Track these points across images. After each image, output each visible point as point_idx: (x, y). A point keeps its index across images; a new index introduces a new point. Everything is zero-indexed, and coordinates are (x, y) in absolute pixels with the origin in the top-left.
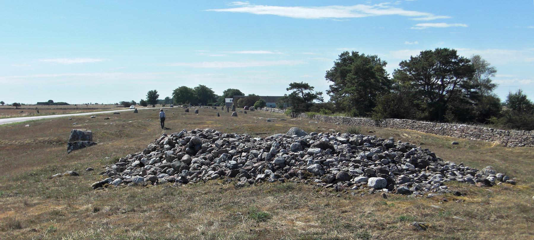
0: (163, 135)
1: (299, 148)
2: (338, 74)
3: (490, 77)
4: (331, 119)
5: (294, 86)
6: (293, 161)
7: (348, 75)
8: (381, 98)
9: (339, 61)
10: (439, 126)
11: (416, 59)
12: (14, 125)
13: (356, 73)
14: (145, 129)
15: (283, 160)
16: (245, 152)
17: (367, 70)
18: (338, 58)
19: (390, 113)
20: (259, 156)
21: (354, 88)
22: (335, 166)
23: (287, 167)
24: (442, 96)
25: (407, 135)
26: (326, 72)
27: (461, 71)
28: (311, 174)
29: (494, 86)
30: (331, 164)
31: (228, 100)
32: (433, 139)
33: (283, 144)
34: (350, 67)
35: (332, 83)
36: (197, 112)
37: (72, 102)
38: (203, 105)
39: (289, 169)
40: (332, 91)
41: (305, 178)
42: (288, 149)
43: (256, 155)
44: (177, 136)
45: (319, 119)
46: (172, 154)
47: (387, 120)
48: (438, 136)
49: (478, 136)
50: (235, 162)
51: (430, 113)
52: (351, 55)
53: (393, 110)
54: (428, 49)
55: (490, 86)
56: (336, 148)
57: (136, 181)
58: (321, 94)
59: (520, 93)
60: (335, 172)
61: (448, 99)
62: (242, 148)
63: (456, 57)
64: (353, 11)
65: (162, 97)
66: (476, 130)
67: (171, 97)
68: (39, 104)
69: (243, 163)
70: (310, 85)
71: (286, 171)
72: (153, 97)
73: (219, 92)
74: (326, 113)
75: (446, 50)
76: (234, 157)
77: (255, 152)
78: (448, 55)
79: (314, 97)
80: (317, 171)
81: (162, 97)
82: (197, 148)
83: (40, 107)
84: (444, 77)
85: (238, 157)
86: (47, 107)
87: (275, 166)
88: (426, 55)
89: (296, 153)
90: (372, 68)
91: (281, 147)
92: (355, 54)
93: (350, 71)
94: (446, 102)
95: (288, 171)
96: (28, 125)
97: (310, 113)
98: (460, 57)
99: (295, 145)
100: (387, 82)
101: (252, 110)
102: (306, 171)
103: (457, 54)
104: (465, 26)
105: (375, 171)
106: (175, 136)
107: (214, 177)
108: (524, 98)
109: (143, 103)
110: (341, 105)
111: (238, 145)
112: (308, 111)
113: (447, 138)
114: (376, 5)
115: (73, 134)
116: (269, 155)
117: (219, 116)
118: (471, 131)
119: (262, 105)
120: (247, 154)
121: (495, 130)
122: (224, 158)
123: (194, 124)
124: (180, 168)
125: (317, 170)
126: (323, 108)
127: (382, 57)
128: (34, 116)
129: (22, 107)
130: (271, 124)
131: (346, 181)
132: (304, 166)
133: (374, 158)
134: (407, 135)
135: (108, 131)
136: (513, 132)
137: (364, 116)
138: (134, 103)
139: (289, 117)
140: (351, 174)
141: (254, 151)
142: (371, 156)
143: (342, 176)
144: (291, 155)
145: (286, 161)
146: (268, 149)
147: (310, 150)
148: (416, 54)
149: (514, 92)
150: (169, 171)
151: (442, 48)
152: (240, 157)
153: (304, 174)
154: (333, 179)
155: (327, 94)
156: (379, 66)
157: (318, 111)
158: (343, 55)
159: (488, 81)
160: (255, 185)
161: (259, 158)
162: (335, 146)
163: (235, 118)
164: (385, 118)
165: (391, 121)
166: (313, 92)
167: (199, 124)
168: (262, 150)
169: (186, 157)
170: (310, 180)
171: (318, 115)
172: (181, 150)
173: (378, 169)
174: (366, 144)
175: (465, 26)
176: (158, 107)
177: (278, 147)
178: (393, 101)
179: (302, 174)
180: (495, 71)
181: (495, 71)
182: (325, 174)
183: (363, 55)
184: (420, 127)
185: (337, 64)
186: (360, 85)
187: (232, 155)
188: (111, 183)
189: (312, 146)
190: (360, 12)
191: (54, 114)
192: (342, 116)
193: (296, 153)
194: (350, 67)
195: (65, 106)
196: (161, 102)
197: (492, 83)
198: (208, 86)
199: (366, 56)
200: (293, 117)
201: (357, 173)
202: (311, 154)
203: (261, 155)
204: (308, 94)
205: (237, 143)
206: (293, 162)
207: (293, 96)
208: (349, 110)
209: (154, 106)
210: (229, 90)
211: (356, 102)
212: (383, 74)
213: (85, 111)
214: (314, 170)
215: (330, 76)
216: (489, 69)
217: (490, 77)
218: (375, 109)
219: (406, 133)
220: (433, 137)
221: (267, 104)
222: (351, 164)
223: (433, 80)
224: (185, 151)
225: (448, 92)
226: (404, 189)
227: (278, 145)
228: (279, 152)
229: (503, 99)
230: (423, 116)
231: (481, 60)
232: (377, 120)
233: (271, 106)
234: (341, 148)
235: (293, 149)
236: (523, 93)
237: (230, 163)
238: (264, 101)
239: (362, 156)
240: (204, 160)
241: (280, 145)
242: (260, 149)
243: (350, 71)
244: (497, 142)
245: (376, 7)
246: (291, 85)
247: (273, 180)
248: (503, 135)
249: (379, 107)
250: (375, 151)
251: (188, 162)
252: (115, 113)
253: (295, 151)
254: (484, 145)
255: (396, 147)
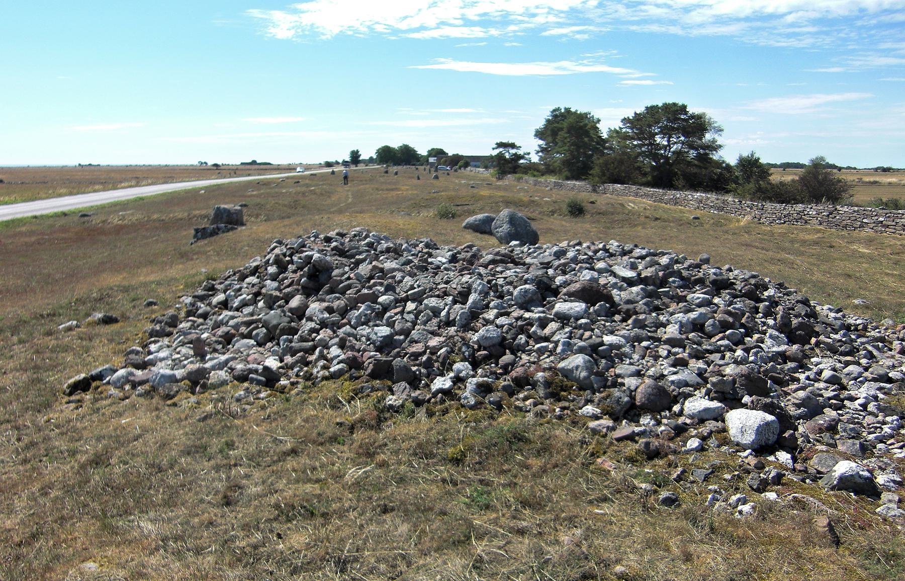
0: (276, 242)
1: (535, 298)
2: (549, 132)
3: (716, 136)
4: (540, 182)
5: (500, 145)
6: (522, 339)
7: (560, 133)
8: (598, 161)
9: (550, 118)
10: (670, 194)
11: (640, 114)
12: (187, 192)
13: (569, 132)
14: (329, 197)
15: (498, 336)
16: (413, 301)
17: (581, 128)
18: (549, 114)
19: (609, 178)
20: (443, 313)
21: (566, 148)
22: (626, 357)
23: (508, 357)
24: (667, 158)
25: (632, 205)
26: (596, 117)
27: (690, 130)
28: (569, 383)
29: (720, 146)
30: (616, 354)
31: (431, 160)
32: (665, 210)
33: (496, 285)
34: (562, 124)
35: (541, 142)
36: (396, 173)
37: (275, 161)
38: (406, 164)
39: (513, 364)
40: (541, 151)
41: (555, 396)
42: (509, 300)
43: (436, 312)
44: (293, 248)
45: (527, 182)
46: (276, 289)
47: (606, 185)
48: (668, 206)
49: (720, 209)
50: (389, 329)
51: (653, 177)
52: (563, 111)
53: (613, 173)
54: (655, 104)
55: (714, 147)
56: (617, 299)
57: (155, 380)
58: (529, 154)
59: (752, 155)
60: (631, 382)
61: (674, 162)
62: (406, 292)
63: (686, 113)
64: (557, 68)
65: (364, 156)
66: (719, 201)
67: (375, 157)
68: (242, 164)
69: (407, 333)
70: (517, 144)
71: (506, 369)
72: (355, 157)
73: (422, 151)
74: (534, 176)
75: (675, 104)
76: (388, 314)
77: (434, 304)
78: (677, 110)
79: (522, 157)
80: (585, 378)
81: (364, 156)
82: (322, 278)
83: (243, 167)
84: (670, 137)
85: (396, 314)
86: (249, 167)
87: (479, 350)
88: (651, 110)
89: (527, 315)
90: (586, 125)
91: (492, 294)
92: (568, 110)
93: (562, 129)
94: (671, 165)
95: (512, 370)
96: (203, 192)
97: (517, 175)
98: (691, 112)
99: (526, 291)
100: (604, 141)
101: (456, 171)
102: (557, 375)
103: (687, 110)
104: (671, 83)
105: (734, 381)
106: (290, 248)
107: (335, 372)
108: (757, 160)
109: (345, 163)
110: (551, 168)
111: (401, 281)
112: (515, 173)
113: (681, 209)
114: (581, 62)
115: (216, 212)
116: (464, 316)
117: (419, 178)
118: (712, 202)
119: (466, 165)
120: (417, 307)
121: (744, 202)
122: (366, 315)
123: (387, 190)
124: (278, 331)
125: (584, 374)
126: (531, 168)
127: (596, 114)
128: (225, 177)
129: (222, 167)
130: (475, 191)
131: (663, 414)
132: (549, 356)
133: (710, 328)
134: (632, 205)
135: (280, 202)
136: (768, 205)
137: (576, 180)
138: (337, 163)
139: (494, 179)
140: (674, 390)
141: (432, 302)
142: (701, 321)
143: (652, 397)
144: (517, 319)
145: (504, 339)
146: (462, 297)
147: (561, 306)
148: (641, 110)
149: (745, 154)
150: (257, 334)
151: (671, 102)
152: (402, 312)
153: (552, 383)
154: (628, 406)
155: (536, 154)
156: (593, 124)
157: (526, 173)
158: (554, 111)
159: (714, 141)
160: (430, 414)
161: (444, 319)
162: (615, 292)
163: (435, 182)
164: (604, 183)
165: (611, 187)
166: (521, 152)
167: (392, 190)
168: (451, 298)
169: (295, 302)
170: (567, 404)
171: (526, 177)
172: (293, 281)
173: (742, 376)
174: (674, 282)
175: (671, 83)
176: (361, 167)
177: (487, 294)
178: (613, 163)
179: (548, 384)
180: (722, 130)
181: (722, 130)
182: (605, 387)
183: (577, 111)
184: (646, 195)
185: (548, 121)
186: (572, 145)
187: (386, 309)
188: (108, 379)
189: (565, 295)
190: (564, 69)
191: (249, 175)
192: (552, 179)
193: (527, 315)
194: (562, 124)
195: (269, 166)
196: (364, 161)
197: (717, 143)
198: (411, 145)
199: (578, 112)
200: (499, 179)
201: (687, 384)
202: (563, 319)
203: (448, 313)
204: (515, 154)
205: (399, 275)
206: (523, 341)
207: (500, 157)
208: (560, 171)
209: (356, 166)
210: (433, 149)
211: (566, 163)
212: (597, 132)
213: (284, 171)
214: (577, 373)
215: (539, 134)
216: (714, 128)
217: (716, 136)
218: (591, 172)
219: (630, 202)
220: (663, 207)
221: (472, 163)
222: (663, 351)
223: (658, 139)
224: (299, 285)
225: (673, 152)
226: (860, 476)
227: (486, 289)
228: (487, 306)
229: (732, 161)
230: (644, 180)
231: (707, 117)
232: (593, 186)
233: (476, 166)
234: (628, 297)
235: (520, 301)
236: (756, 156)
237: (376, 334)
238: (469, 160)
239: (681, 322)
240: (326, 315)
241: (490, 288)
242: (446, 294)
243: (562, 129)
244: (748, 218)
245: (581, 64)
246: (497, 144)
247: (472, 402)
248: (755, 208)
249: (596, 171)
250: (698, 301)
251: (300, 314)
252: (312, 175)
253: (525, 306)
254: (730, 220)
255: (736, 287)
